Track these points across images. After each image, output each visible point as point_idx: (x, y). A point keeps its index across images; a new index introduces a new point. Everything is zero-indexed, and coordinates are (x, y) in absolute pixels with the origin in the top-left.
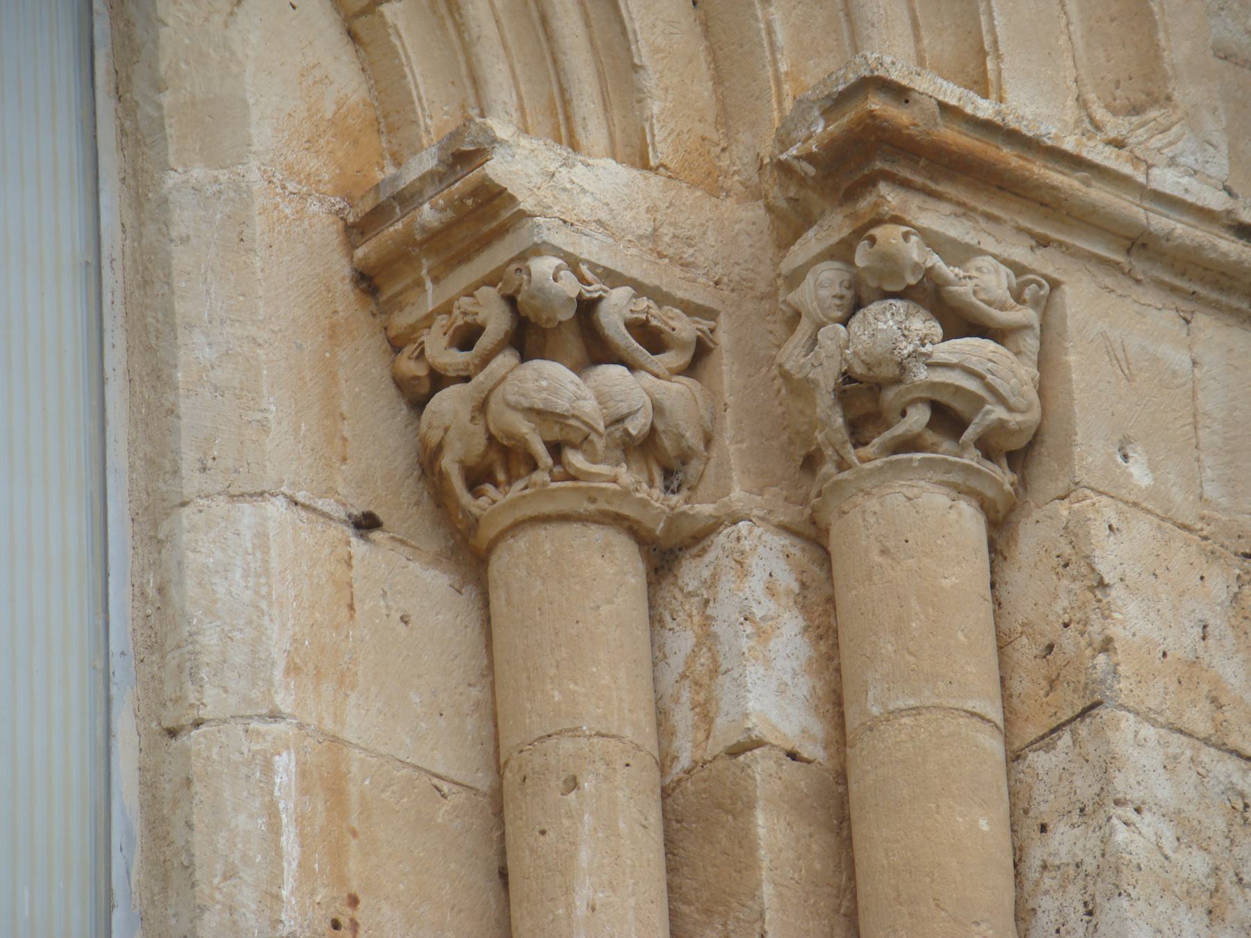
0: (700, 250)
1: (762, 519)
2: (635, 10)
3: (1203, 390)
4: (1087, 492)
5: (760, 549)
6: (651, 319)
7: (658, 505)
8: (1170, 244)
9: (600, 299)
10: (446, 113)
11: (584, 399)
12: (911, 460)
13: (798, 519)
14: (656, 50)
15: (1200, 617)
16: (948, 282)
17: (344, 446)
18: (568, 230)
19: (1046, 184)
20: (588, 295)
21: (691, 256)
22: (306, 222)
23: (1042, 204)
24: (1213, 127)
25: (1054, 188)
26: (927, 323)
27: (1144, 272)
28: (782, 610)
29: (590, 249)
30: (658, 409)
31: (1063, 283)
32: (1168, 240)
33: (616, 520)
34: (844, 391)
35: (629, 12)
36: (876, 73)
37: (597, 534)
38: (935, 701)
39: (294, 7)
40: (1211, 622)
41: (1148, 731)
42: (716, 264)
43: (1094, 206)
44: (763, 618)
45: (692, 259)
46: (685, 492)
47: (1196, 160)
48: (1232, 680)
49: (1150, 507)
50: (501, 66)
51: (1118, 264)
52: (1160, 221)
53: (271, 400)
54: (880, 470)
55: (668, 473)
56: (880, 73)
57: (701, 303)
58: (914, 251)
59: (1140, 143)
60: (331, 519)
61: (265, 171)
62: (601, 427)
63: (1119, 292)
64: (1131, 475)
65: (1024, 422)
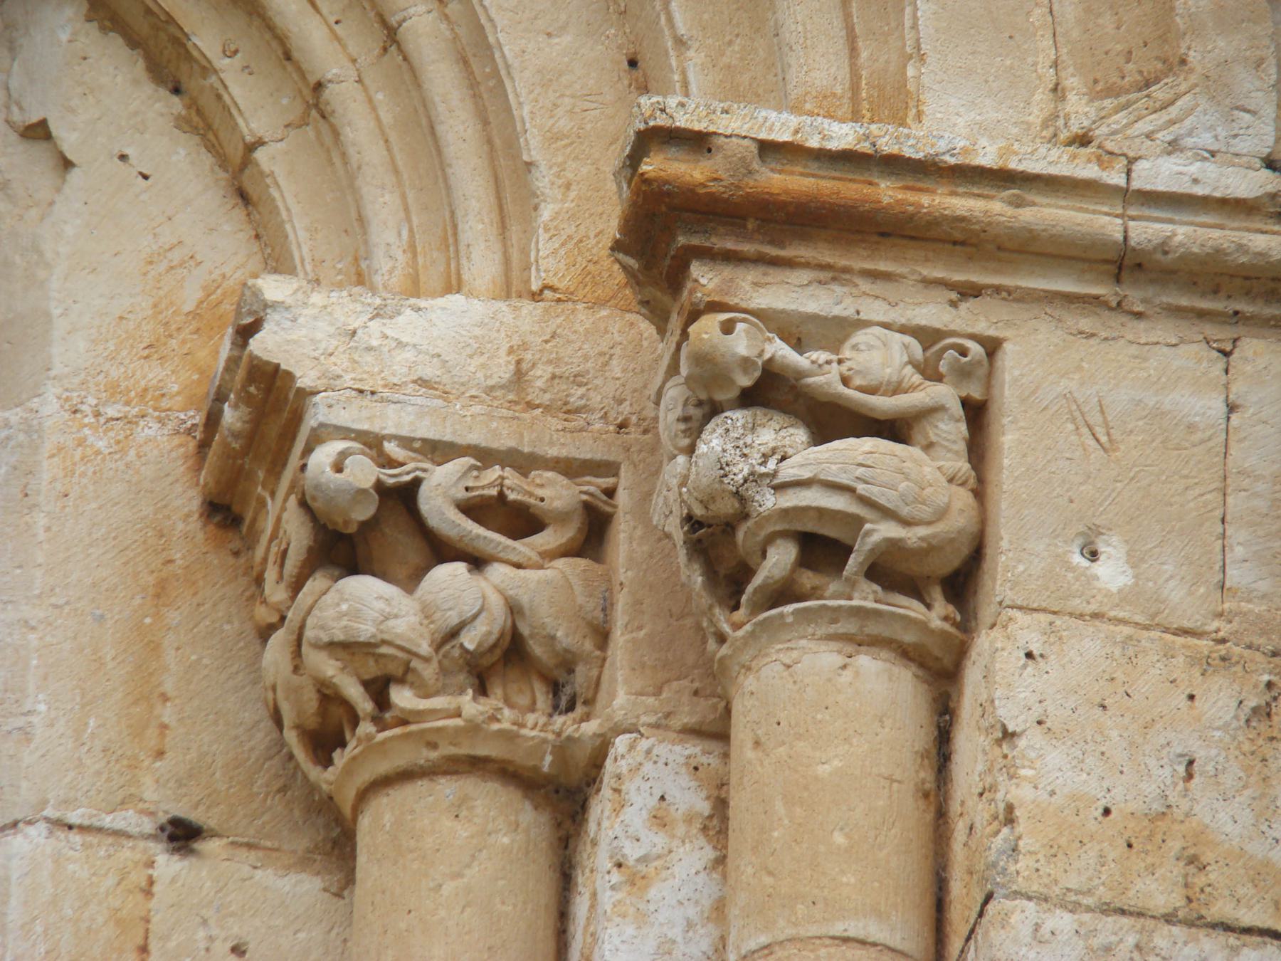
0: (596, 388)
1: (656, 726)
2: (524, 92)
3: (1240, 441)
4: (1011, 612)
5: (648, 768)
6: (508, 492)
7: (533, 733)
8: (1170, 256)
9: (417, 482)
10: (340, 272)
11: (396, 616)
12: (782, 616)
13: (712, 717)
14: (553, 138)
15: (1179, 750)
16: (801, 374)
17: (162, 735)
18: (366, 400)
19: (945, 217)
20: (391, 481)
21: (581, 398)
22: (132, 453)
23: (955, 243)
24: (1255, 88)
25: (962, 219)
26: (783, 433)
27: (1144, 301)
28: (676, 843)
29: (394, 420)
30: (514, 609)
31: (1004, 340)
32: (1166, 253)
33: (475, 765)
34: (699, 541)
35: (517, 95)
36: (652, 123)
37: (447, 788)
38: (791, 932)
39: (146, 177)
40: (1200, 755)
41: (1062, 921)
42: (620, 402)
43: (1031, 231)
44: (644, 859)
45: (583, 402)
46: (580, 710)
47: (1216, 137)
48: (1229, 828)
49: (1121, 615)
50: (387, 197)
51: (1097, 298)
52: (1148, 231)
53: (41, 697)
54: (752, 634)
55: (555, 688)
56: (661, 121)
57: (588, 456)
58: (741, 344)
59: (1114, 133)
60: (129, 836)
61: (67, 399)
62: (425, 648)
63: (1104, 334)
64: (1097, 578)
65: (934, 536)
